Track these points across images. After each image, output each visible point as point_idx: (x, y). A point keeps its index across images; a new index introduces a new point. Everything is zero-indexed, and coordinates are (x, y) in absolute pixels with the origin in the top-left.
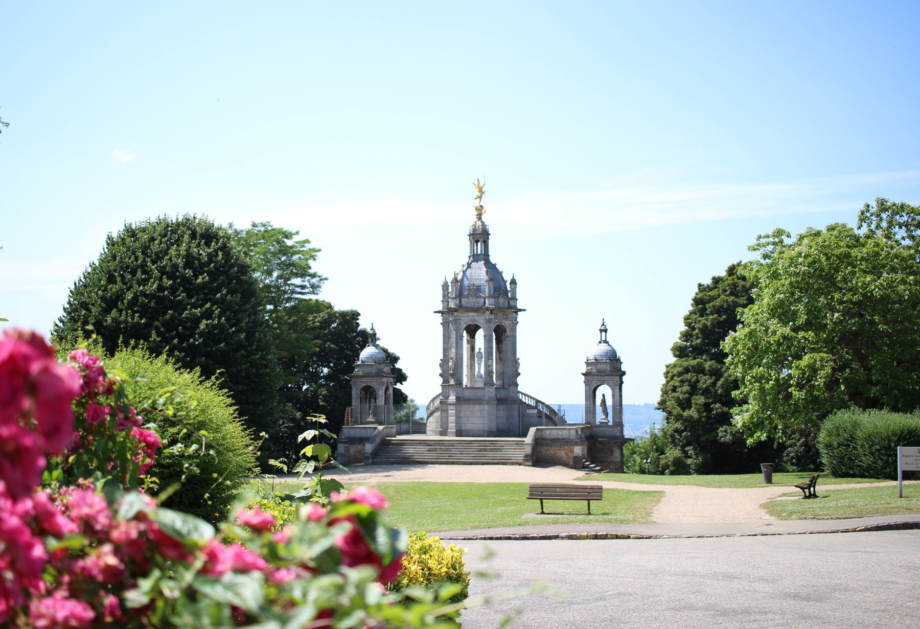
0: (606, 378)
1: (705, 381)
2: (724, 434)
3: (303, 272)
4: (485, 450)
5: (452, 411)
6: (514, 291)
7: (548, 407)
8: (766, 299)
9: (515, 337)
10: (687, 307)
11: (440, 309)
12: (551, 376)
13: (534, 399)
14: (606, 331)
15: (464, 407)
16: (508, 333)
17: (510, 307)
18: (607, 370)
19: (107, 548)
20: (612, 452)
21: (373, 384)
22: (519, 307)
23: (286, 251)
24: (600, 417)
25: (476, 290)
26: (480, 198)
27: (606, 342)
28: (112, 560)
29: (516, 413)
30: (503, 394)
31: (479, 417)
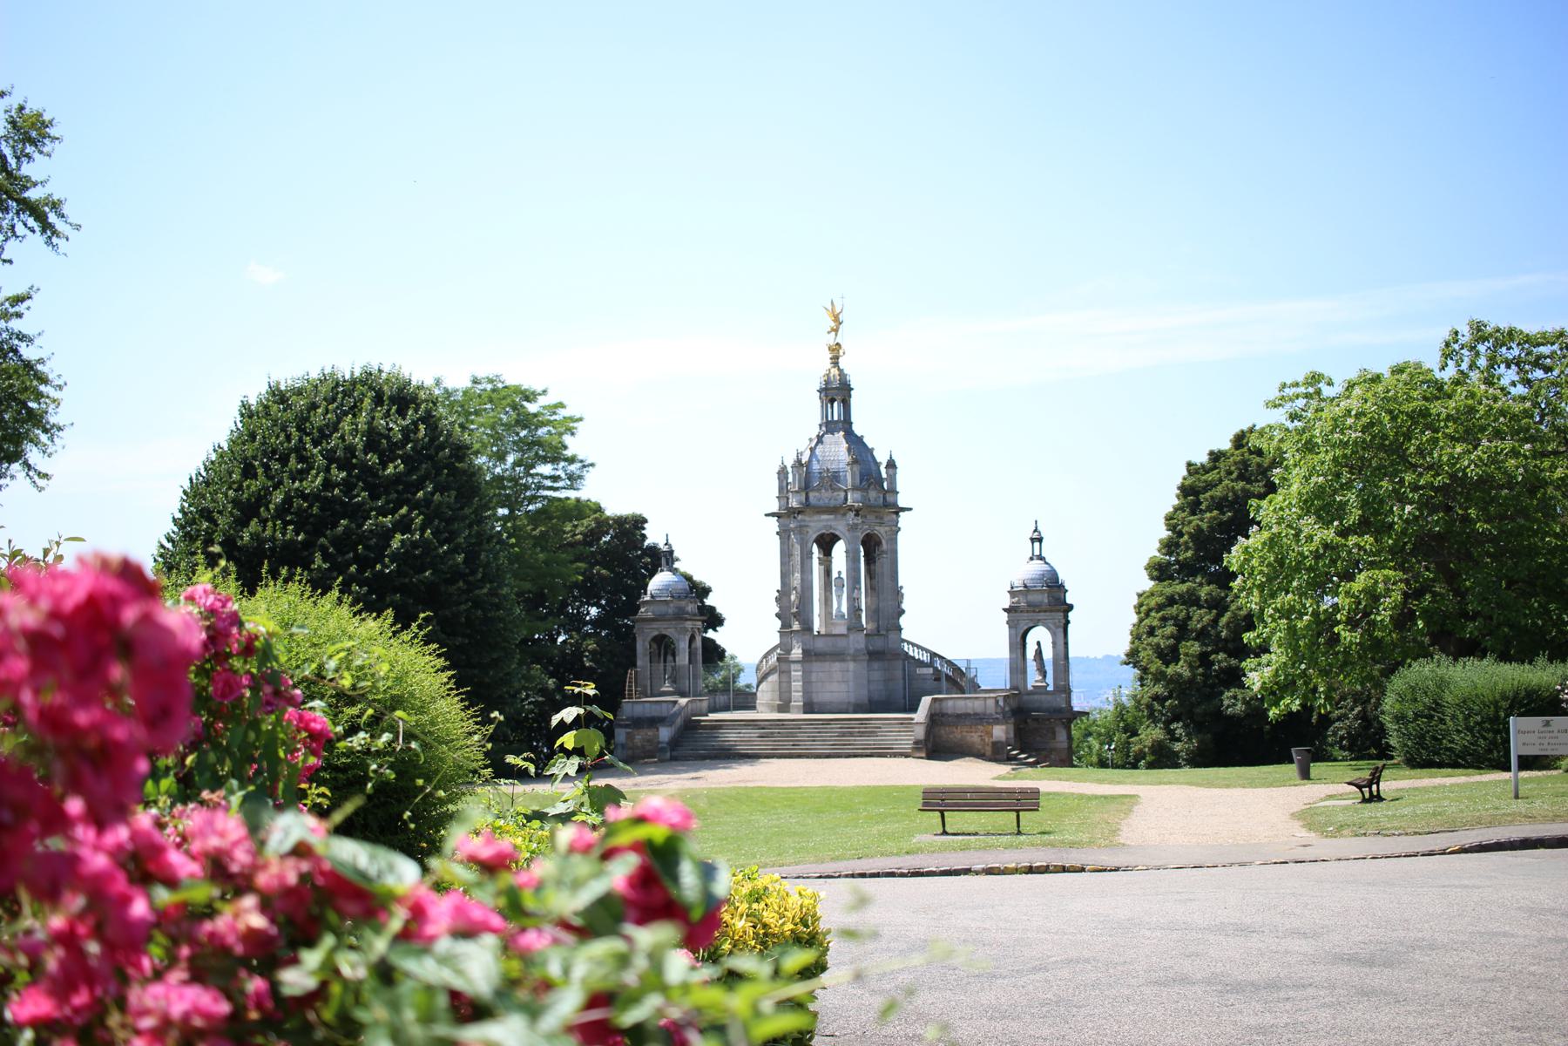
0: (1042, 616)
1: (1200, 618)
3: (555, 454)
4: (851, 734)
5: (797, 673)
6: (892, 479)
7: (949, 663)
8: (1295, 484)
9: (895, 552)
10: (1170, 500)
11: (775, 509)
12: (953, 613)
13: (927, 651)
14: (1040, 540)
15: (816, 666)
16: (885, 546)
17: (886, 505)
18: (1043, 602)
19: (249, 901)
20: (1054, 733)
21: (670, 632)
22: (901, 504)
24: (1033, 678)
25: (834, 478)
26: (836, 330)
27: (1040, 558)
28: (258, 921)
29: (899, 673)
30: (878, 643)
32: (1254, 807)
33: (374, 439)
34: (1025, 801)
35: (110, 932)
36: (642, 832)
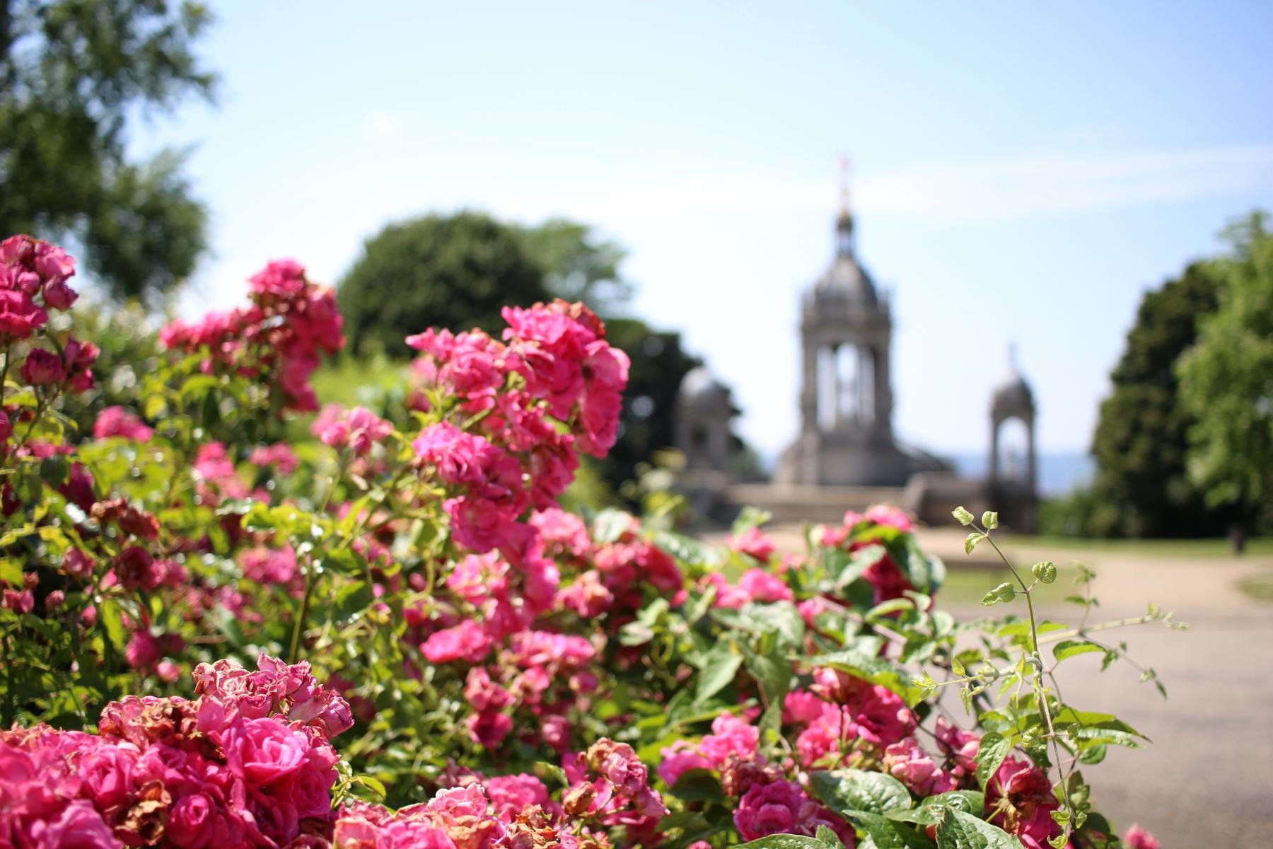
1: (1151, 419)
2: (1177, 491)
3: (608, 274)
8: (1237, 305)
12: (940, 415)
18: (1016, 403)
19: (591, 576)
23: (585, 250)
28: (601, 591)
31: (847, 465)
32: (1194, 578)
33: (470, 265)
34: (1001, 568)
35: (529, 590)
36: (878, 532)
